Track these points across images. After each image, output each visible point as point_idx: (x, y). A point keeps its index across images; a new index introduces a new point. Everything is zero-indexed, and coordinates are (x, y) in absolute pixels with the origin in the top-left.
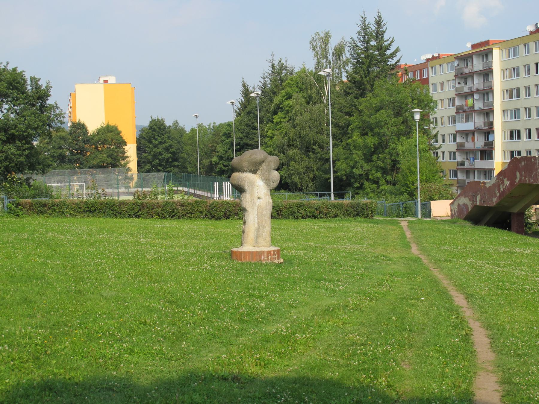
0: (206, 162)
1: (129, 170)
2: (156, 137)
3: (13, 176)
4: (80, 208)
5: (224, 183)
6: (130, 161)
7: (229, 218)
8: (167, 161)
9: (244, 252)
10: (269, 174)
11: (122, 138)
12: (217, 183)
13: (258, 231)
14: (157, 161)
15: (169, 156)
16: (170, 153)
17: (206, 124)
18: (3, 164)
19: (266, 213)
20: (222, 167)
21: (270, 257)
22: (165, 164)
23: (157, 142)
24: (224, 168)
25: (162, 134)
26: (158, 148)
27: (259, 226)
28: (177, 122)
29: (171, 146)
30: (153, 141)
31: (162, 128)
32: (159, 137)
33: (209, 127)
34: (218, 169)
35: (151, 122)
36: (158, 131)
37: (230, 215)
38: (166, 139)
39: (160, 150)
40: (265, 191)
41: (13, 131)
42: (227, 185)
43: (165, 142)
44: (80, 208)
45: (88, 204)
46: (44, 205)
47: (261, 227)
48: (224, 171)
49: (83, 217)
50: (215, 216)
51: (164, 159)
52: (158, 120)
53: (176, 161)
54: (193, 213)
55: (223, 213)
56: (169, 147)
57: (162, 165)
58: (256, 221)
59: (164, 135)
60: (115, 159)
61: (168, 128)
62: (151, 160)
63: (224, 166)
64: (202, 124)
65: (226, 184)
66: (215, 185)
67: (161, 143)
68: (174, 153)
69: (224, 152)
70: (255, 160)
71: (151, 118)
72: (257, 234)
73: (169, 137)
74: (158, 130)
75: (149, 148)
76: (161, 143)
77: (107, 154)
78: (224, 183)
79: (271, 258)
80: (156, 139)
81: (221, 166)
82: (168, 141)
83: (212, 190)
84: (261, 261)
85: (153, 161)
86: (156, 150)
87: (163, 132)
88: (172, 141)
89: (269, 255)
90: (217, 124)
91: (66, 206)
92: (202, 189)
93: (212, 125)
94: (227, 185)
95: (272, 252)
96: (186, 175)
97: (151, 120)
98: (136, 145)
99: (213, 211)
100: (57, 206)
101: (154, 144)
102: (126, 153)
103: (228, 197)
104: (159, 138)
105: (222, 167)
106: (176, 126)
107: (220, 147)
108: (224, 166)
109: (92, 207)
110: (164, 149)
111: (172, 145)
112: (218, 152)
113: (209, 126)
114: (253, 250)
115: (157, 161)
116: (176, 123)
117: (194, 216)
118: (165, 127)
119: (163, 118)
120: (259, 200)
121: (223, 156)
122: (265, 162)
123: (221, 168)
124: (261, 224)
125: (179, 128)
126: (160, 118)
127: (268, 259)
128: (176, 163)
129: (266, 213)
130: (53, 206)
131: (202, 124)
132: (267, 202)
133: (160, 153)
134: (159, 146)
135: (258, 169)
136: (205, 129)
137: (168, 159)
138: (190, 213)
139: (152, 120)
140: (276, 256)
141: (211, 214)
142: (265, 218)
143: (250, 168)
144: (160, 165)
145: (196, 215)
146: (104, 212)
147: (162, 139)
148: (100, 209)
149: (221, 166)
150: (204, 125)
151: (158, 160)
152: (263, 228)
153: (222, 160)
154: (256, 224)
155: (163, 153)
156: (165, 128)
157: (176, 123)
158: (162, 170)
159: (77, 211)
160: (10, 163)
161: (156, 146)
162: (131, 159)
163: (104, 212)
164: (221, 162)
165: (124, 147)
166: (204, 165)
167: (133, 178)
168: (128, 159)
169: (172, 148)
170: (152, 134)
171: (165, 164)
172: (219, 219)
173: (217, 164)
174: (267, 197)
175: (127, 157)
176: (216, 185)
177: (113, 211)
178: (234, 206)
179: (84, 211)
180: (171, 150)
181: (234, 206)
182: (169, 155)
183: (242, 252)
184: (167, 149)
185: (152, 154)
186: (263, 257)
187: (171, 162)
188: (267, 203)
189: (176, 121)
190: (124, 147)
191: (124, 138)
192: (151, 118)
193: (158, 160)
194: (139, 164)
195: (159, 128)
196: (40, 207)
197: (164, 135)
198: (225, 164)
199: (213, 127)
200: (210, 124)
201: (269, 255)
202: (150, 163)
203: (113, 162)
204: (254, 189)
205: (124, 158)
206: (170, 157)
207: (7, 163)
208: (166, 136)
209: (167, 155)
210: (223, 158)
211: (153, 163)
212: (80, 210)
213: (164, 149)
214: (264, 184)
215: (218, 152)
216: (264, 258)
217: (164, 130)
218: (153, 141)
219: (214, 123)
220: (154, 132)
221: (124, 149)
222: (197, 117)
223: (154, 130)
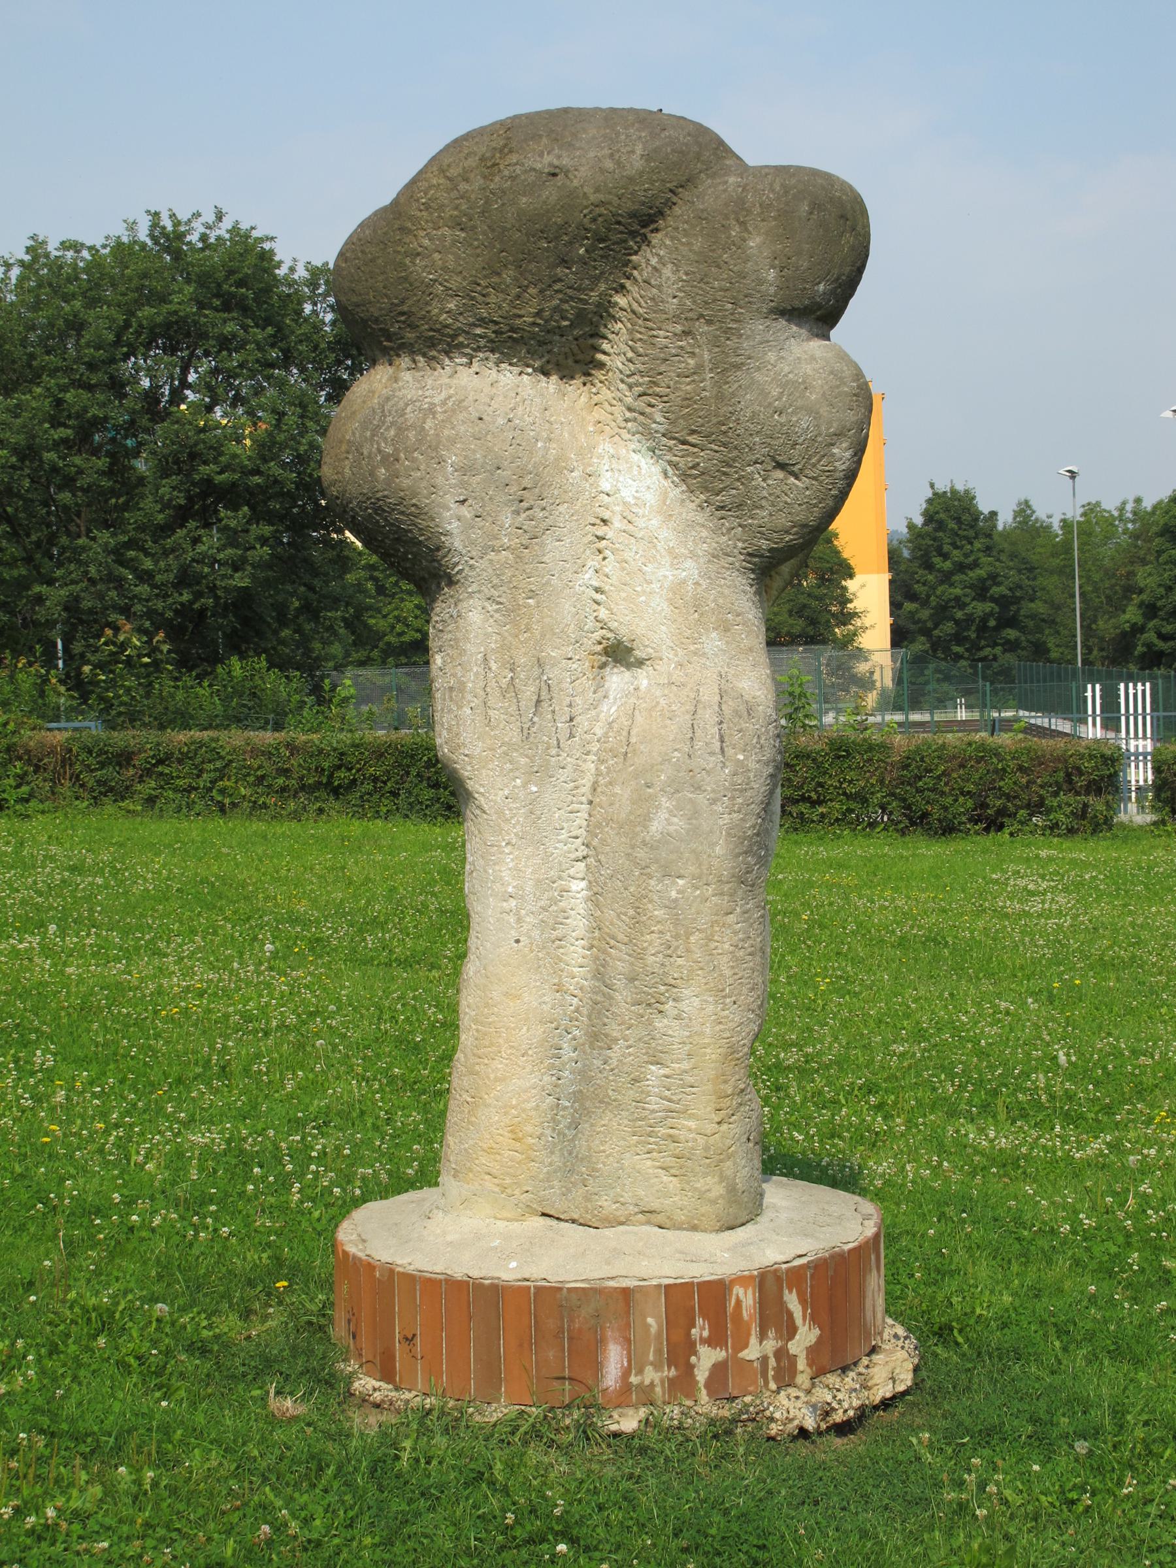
0: (1107, 627)
1: (861, 654)
2: (946, 548)
3: (122, 638)
4: (285, 772)
5: (1122, 686)
6: (864, 629)
7: (1000, 828)
8: (983, 628)
9: (410, 1279)
10: (727, 367)
11: (838, 552)
12: (1098, 687)
13: (597, 1038)
14: (949, 627)
15: (988, 610)
16: (993, 600)
17: (1110, 505)
18: (170, 600)
19: (678, 824)
20: (1156, 641)
21: (706, 1359)
22: (973, 636)
23: (948, 565)
24: (1161, 645)
25: (966, 538)
26: (952, 585)
27: (600, 973)
28: (1029, 507)
29: (994, 578)
30: (937, 560)
31: (966, 517)
32: (956, 547)
33: (1121, 515)
34: (1140, 649)
35: (929, 501)
36: (952, 529)
37: (1002, 812)
38: (981, 554)
39: (958, 591)
40: (690, 570)
41: (205, 470)
42: (1135, 695)
43: (975, 565)
44: (285, 772)
45: (321, 751)
46: (124, 758)
47: (622, 996)
48: (1161, 654)
49: (296, 816)
50: (925, 815)
51: (970, 619)
52: (954, 492)
53: (1011, 627)
54: (819, 802)
55: (970, 804)
56: (989, 582)
57: (966, 638)
58: (578, 924)
59: (971, 543)
60: (813, 622)
61: (986, 520)
62: (930, 624)
63: (1163, 637)
64: (1098, 504)
65: (1131, 691)
66: (1089, 694)
67: (961, 568)
68: (1001, 601)
69: (1162, 590)
70: (550, 194)
71: (932, 486)
72: (584, 1075)
73: (988, 550)
74: (952, 525)
75: (924, 584)
76: (961, 568)
77: (787, 607)
78: (1122, 686)
79: (719, 1371)
80: (945, 556)
81: (1150, 636)
82: (984, 560)
83: (1075, 710)
84: (592, 1407)
85: (936, 626)
86: (943, 593)
87: (971, 533)
88: (998, 560)
89: (700, 1330)
90: (1148, 504)
91: (218, 764)
92: (1048, 708)
93: (1129, 507)
94: (1135, 695)
95: (746, 1298)
96: (1031, 667)
97: (929, 494)
98: (886, 577)
99: (919, 791)
100: (180, 761)
101: (939, 571)
102: (851, 601)
103: (1136, 737)
104: (955, 552)
105: (1156, 641)
106: (1025, 521)
107: (1150, 574)
108: (1163, 637)
109: (339, 767)
110: (971, 587)
111: (998, 575)
112: (1141, 591)
113: (1121, 509)
114: (509, 1271)
115: (949, 627)
116: (1024, 510)
117: (823, 816)
118: (976, 516)
119: (970, 486)
120: (617, 679)
121: (1159, 604)
122: (668, 222)
123: (1149, 646)
124: (620, 965)
125: (1033, 525)
126: (960, 487)
127: (683, 1383)
128: (1011, 634)
129: (678, 824)
130: (160, 762)
131: (1098, 504)
132: (710, 695)
133: (959, 603)
134: (956, 578)
135: (604, 312)
136: (1109, 522)
137: (984, 620)
138: (804, 799)
139: (935, 494)
140: (806, 1336)
141: (909, 807)
142: (676, 889)
143: (496, 304)
144: (959, 639)
145: (836, 807)
146: (395, 794)
147: (966, 556)
148: (375, 779)
149: (1150, 636)
150: (1104, 506)
151: (951, 624)
152: (655, 1004)
153: (1155, 616)
154: (576, 953)
155: (968, 600)
156: (977, 519)
157: (1024, 510)
158: (966, 654)
159: (269, 786)
160: (198, 595)
161: (946, 578)
162: (867, 621)
163: (395, 794)
164: (1151, 625)
165: (843, 583)
166: (1102, 639)
167: (873, 682)
168: (858, 622)
169: (999, 584)
170: (934, 539)
171: (973, 636)
172: (948, 830)
173: (1137, 629)
174: (713, 642)
175: (855, 615)
176: (1093, 693)
177: (436, 785)
178: (1021, 768)
179: (303, 788)
180: (996, 590)
181: (1021, 768)
182: (988, 606)
183: (390, 1271)
184: (981, 591)
185: (934, 604)
186: (614, 1360)
187: (997, 629)
188: (708, 716)
189: (1026, 502)
190: (843, 583)
191: (845, 555)
192: (932, 486)
193: (951, 624)
194: (899, 637)
195: (958, 520)
196: (103, 765)
197: (971, 543)
198: (1164, 631)
199: (1135, 513)
200: (1124, 503)
201: (700, 1330)
202: (926, 632)
203: (810, 631)
204: (554, 549)
205: (846, 617)
206: (991, 614)
207: (186, 597)
208: (977, 545)
209: (981, 608)
210: (1160, 609)
211: (936, 632)
212: (281, 781)
213: (971, 587)
214: (676, 492)
215: (1141, 591)
216: (633, 1364)
217: (972, 527)
218: (937, 560)
219: (1138, 501)
220: (941, 534)
221: (845, 589)
222: (1073, 475)
223: (941, 526)
